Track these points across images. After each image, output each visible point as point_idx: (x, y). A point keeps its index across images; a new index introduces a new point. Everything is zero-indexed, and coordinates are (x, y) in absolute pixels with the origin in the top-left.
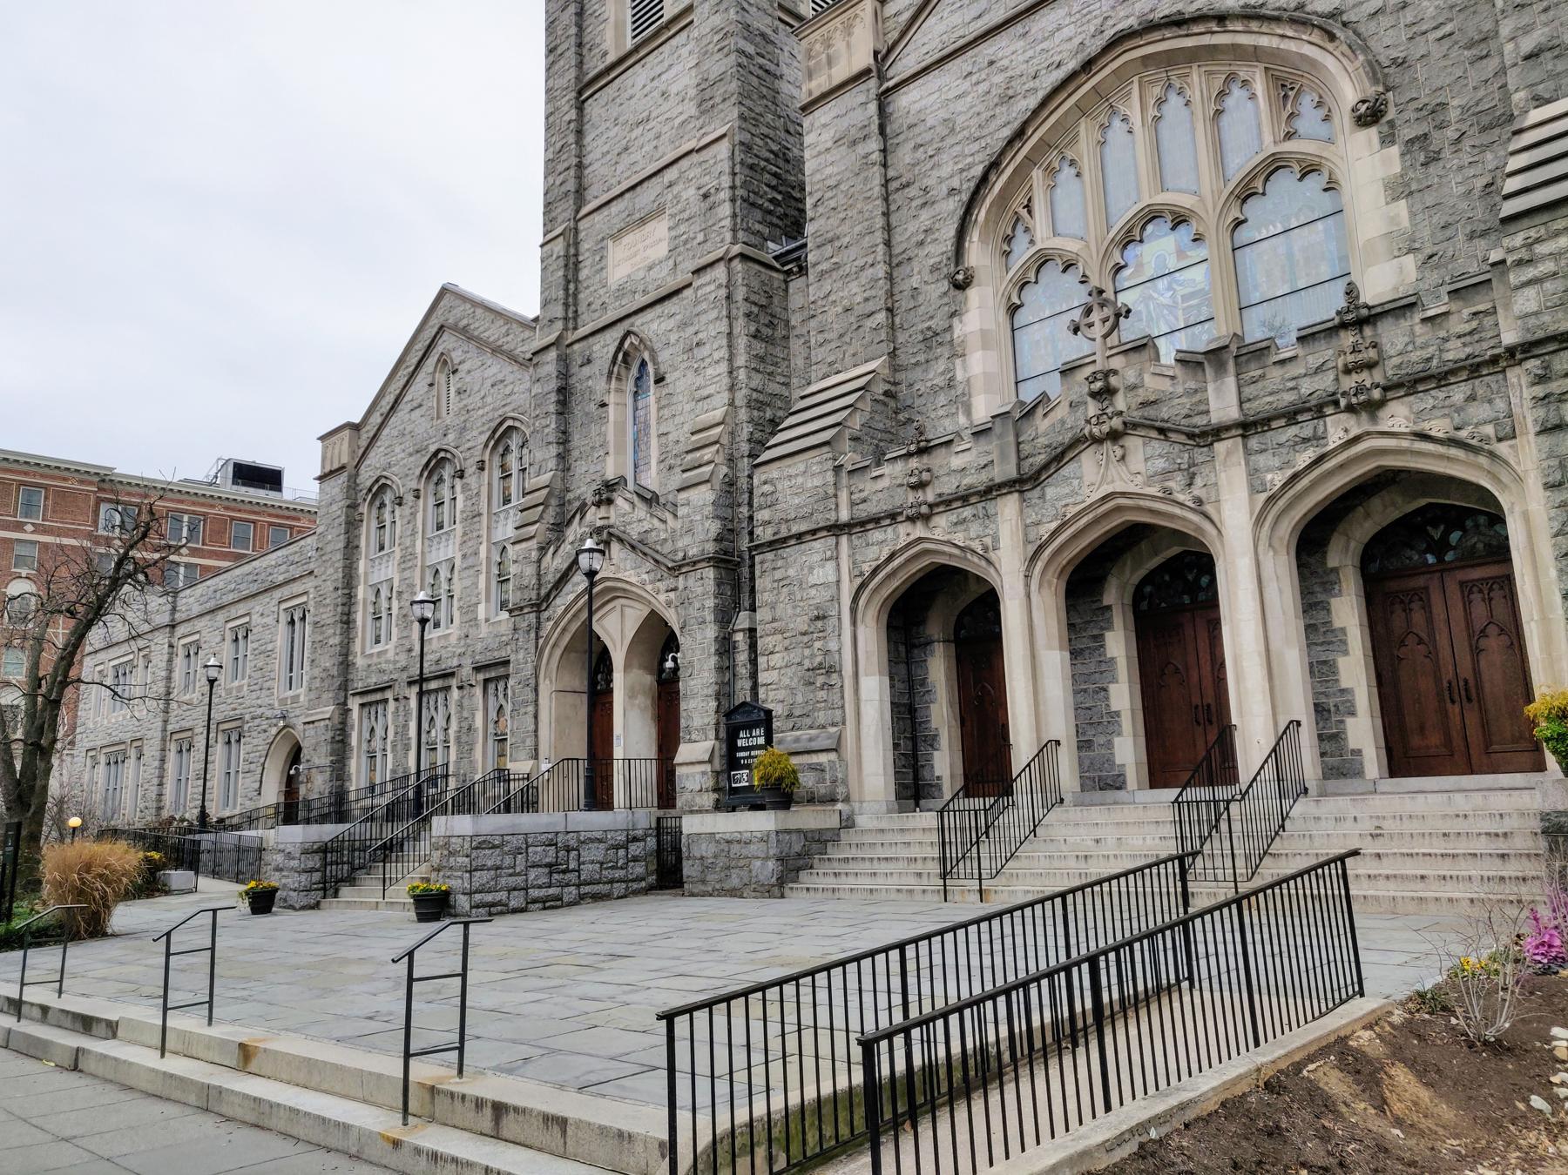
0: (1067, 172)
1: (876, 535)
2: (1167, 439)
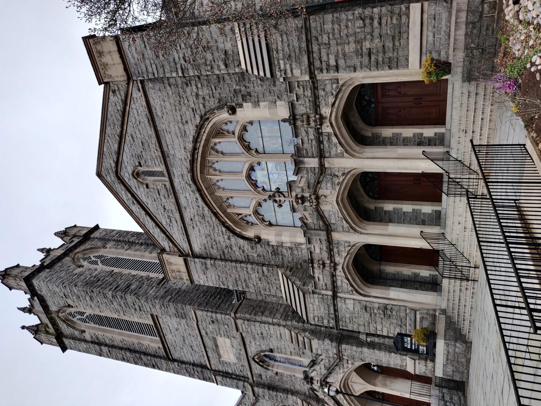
0: (230, 201)
1: (339, 283)
2: (321, 182)
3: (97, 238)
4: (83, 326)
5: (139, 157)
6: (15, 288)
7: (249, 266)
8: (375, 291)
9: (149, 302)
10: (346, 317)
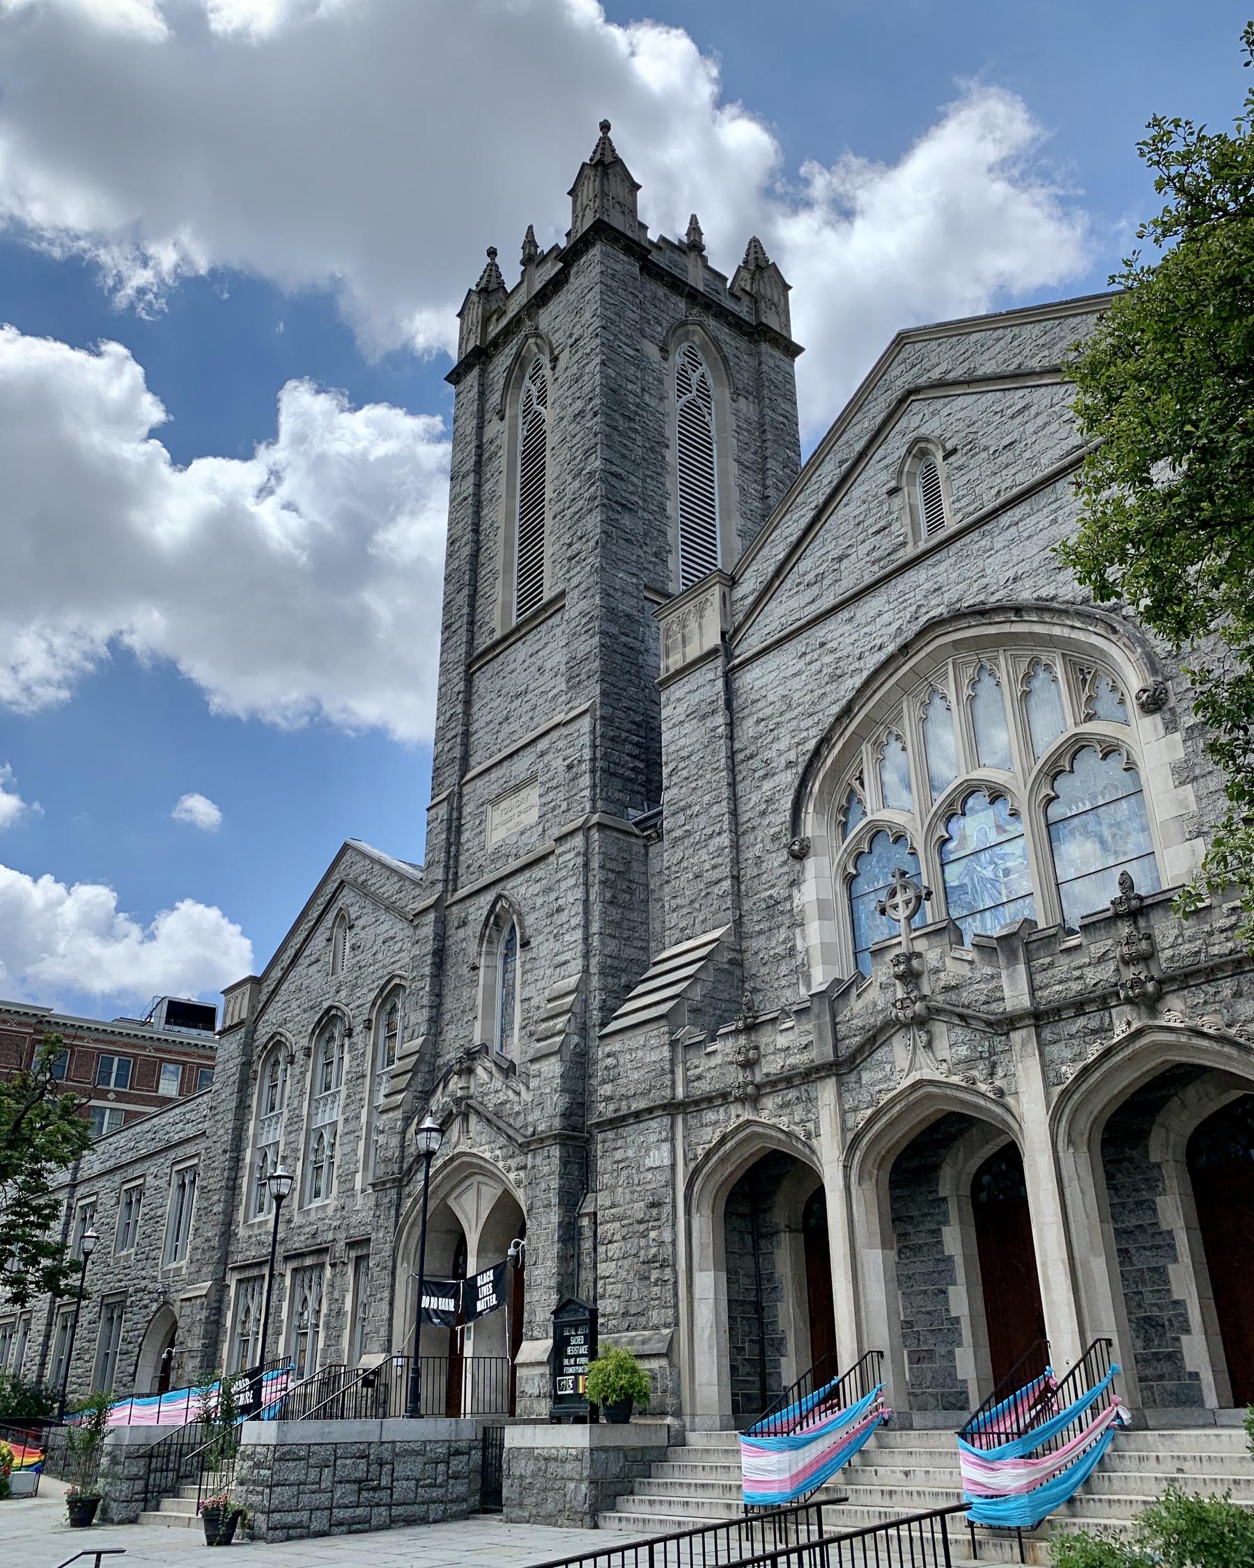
0: (895, 746)
1: (710, 1116)
2: (968, 1025)
4: (515, 410)
5: (972, 446)
6: (575, 202)
7: (725, 840)
8: (703, 1225)
9: (591, 579)
10: (626, 1147)
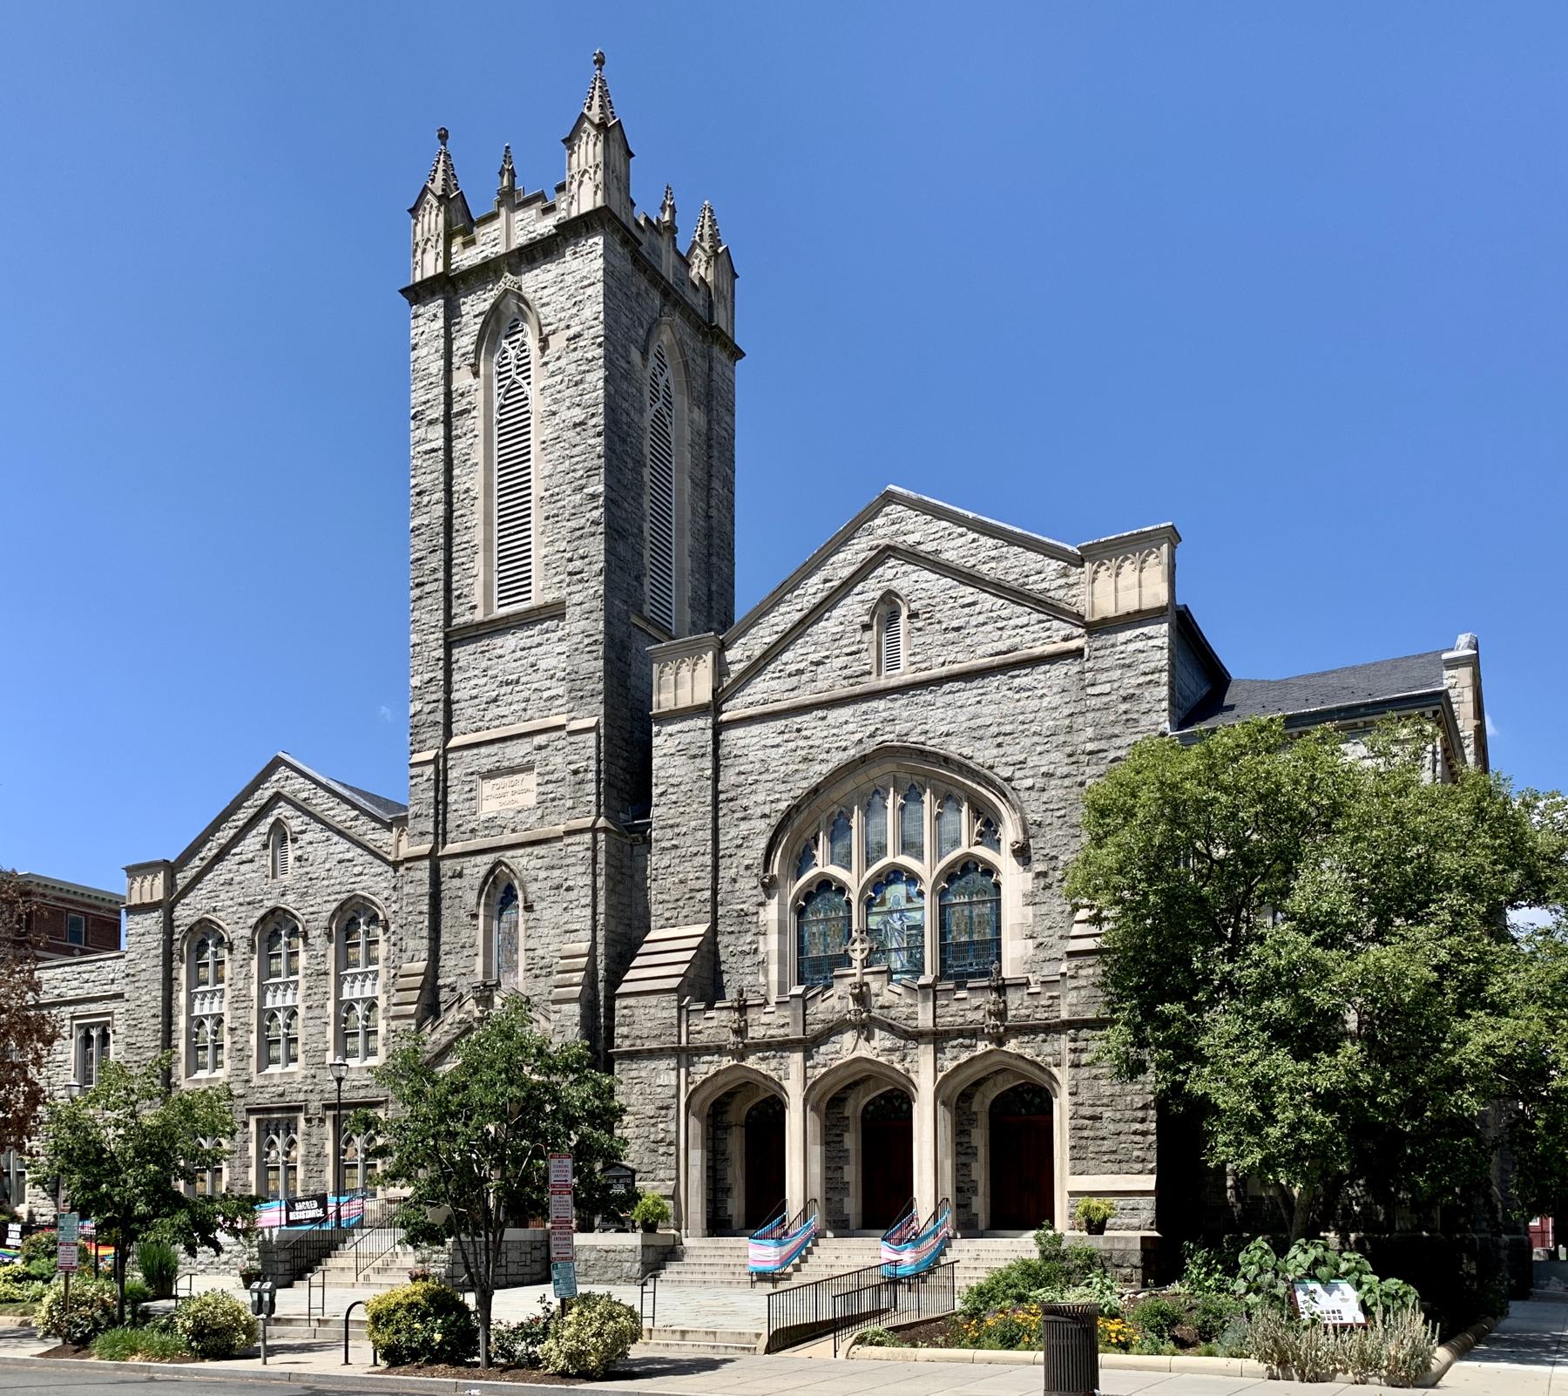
3: (711, 369)
